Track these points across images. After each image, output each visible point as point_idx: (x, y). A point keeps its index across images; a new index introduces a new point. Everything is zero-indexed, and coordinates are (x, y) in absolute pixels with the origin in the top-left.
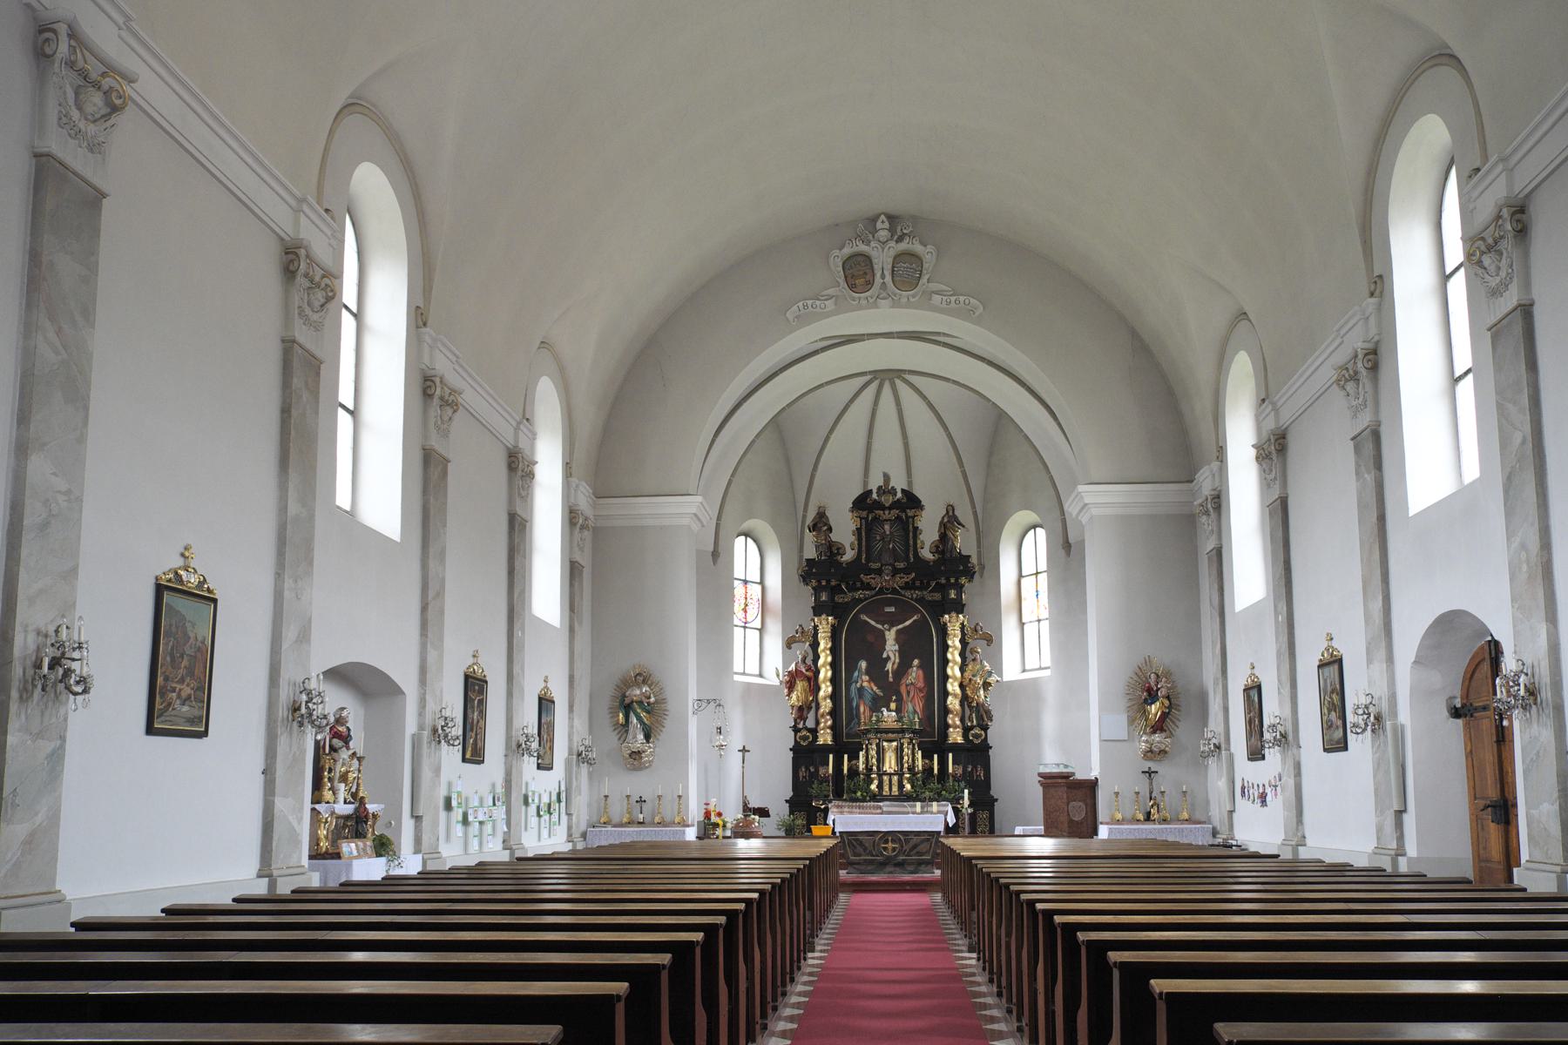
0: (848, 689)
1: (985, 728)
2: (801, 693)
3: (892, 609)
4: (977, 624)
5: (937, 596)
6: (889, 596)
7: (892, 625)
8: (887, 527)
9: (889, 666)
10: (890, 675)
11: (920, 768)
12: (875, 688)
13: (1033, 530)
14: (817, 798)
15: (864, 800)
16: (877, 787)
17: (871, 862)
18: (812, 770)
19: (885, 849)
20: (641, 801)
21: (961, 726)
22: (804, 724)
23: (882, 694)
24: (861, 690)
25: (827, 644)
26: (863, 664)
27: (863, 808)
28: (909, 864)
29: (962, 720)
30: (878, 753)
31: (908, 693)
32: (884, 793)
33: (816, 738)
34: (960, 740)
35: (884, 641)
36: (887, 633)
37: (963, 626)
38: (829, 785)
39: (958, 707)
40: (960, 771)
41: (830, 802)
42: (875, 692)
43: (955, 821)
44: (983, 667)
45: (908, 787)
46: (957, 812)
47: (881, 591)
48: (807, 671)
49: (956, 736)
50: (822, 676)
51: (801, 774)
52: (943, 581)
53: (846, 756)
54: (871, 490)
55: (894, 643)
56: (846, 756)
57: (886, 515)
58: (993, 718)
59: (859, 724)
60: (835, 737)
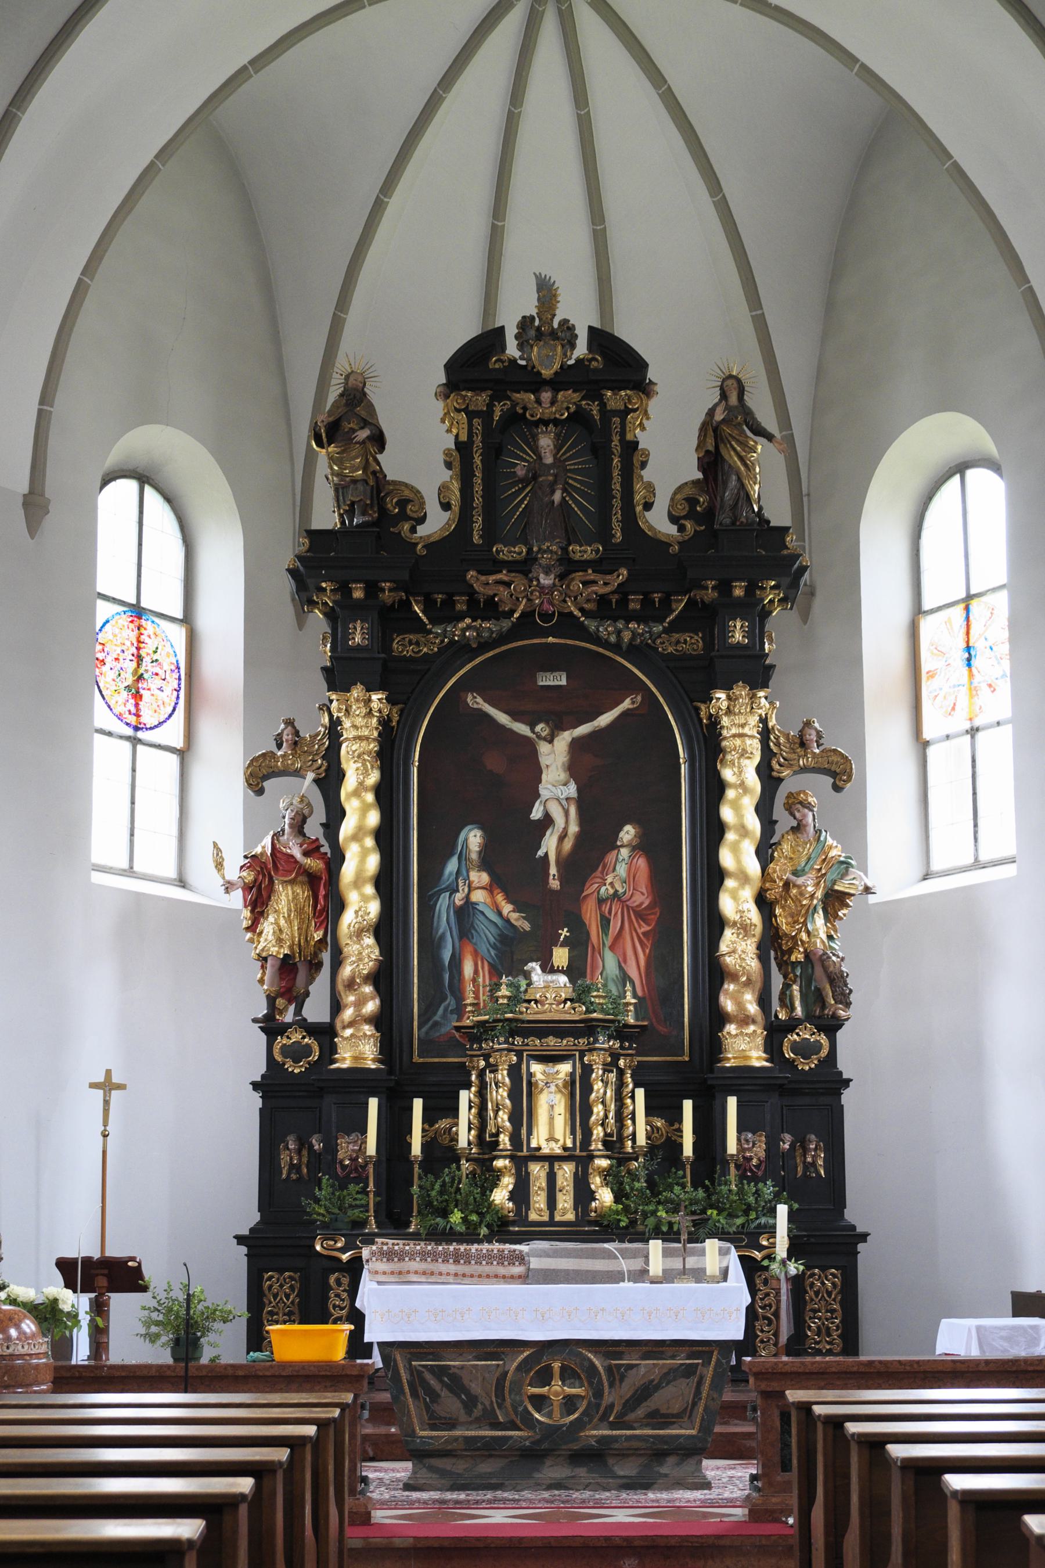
1: (831, 1026)
2: (289, 920)
4: (808, 724)
5: (692, 642)
6: (550, 639)
7: (558, 726)
8: (546, 442)
9: (549, 845)
10: (553, 870)
11: (642, 1140)
12: (507, 908)
13: (957, 478)
14: (330, 1230)
15: (470, 1236)
16: (513, 1196)
17: (488, 1448)
18: (317, 1146)
19: (540, 1402)
21: (760, 1018)
22: (298, 1011)
23: (526, 926)
24: (466, 913)
25: (366, 774)
26: (473, 839)
27: (467, 1258)
28: (623, 1455)
29: (763, 1001)
30: (514, 1094)
31: (605, 922)
32: (533, 1216)
33: (330, 1050)
34: (757, 1058)
36: (543, 748)
37: (765, 733)
38: (364, 1192)
39: (753, 964)
40: (759, 1151)
41: (369, 1240)
42: (507, 921)
43: (749, 1300)
44: (824, 850)
45: (605, 1197)
47: (527, 624)
48: (306, 854)
50: (348, 871)
51: (284, 1158)
52: (710, 594)
53: (418, 1104)
54: (502, 329)
55: (563, 776)
56: (418, 1104)
58: (852, 998)
59: (460, 1011)
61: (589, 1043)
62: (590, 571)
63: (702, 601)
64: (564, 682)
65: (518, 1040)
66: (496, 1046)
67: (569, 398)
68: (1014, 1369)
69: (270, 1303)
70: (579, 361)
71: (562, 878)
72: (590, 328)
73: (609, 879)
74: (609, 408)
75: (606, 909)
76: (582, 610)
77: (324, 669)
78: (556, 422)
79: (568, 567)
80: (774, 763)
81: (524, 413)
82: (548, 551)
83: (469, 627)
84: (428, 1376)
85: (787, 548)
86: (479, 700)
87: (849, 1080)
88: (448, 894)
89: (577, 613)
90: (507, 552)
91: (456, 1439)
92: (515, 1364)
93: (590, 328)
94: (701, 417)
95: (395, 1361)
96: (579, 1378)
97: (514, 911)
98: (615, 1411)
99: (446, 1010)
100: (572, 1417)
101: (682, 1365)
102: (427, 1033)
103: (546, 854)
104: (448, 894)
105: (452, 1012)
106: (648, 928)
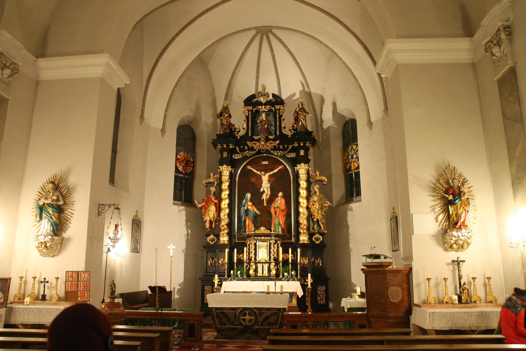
0: (239, 210)
3: (266, 163)
5: (293, 155)
6: (265, 155)
7: (266, 172)
9: (264, 197)
10: (265, 202)
12: (255, 210)
19: (244, 320)
20: (45, 281)
23: (259, 213)
24: (247, 211)
26: (249, 195)
30: (255, 249)
31: (276, 213)
32: (259, 275)
35: (261, 182)
36: (263, 177)
42: (256, 212)
46: (304, 286)
47: (259, 152)
49: (304, 238)
51: (209, 263)
52: (296, 145)
55: (267, 182)
56: (235, 250)
57: (263, 108)
59: (245, 231)
60: (230, 240)
64: (267, 163)
65: (256, 238)
70: (270, 100)
71: (267, 203)
73: (276, 203)
75: (276, 210)
76: (270, 149)
77: (219, 162)
80: (311, 179)
81: (259, 110)
83: (247, 153)
84: (220, 314)
85: (313, 135)
86: (250, 167)
87: (326, 246)
88: (243, 207)
90: (256, 138)
92: (239, 312)
95: (213, 310)
99: (243, 231)
100: (251, 324)
102: (239, 236)
103: (264, 198)
104: (243, 207)
106: (285, 214)
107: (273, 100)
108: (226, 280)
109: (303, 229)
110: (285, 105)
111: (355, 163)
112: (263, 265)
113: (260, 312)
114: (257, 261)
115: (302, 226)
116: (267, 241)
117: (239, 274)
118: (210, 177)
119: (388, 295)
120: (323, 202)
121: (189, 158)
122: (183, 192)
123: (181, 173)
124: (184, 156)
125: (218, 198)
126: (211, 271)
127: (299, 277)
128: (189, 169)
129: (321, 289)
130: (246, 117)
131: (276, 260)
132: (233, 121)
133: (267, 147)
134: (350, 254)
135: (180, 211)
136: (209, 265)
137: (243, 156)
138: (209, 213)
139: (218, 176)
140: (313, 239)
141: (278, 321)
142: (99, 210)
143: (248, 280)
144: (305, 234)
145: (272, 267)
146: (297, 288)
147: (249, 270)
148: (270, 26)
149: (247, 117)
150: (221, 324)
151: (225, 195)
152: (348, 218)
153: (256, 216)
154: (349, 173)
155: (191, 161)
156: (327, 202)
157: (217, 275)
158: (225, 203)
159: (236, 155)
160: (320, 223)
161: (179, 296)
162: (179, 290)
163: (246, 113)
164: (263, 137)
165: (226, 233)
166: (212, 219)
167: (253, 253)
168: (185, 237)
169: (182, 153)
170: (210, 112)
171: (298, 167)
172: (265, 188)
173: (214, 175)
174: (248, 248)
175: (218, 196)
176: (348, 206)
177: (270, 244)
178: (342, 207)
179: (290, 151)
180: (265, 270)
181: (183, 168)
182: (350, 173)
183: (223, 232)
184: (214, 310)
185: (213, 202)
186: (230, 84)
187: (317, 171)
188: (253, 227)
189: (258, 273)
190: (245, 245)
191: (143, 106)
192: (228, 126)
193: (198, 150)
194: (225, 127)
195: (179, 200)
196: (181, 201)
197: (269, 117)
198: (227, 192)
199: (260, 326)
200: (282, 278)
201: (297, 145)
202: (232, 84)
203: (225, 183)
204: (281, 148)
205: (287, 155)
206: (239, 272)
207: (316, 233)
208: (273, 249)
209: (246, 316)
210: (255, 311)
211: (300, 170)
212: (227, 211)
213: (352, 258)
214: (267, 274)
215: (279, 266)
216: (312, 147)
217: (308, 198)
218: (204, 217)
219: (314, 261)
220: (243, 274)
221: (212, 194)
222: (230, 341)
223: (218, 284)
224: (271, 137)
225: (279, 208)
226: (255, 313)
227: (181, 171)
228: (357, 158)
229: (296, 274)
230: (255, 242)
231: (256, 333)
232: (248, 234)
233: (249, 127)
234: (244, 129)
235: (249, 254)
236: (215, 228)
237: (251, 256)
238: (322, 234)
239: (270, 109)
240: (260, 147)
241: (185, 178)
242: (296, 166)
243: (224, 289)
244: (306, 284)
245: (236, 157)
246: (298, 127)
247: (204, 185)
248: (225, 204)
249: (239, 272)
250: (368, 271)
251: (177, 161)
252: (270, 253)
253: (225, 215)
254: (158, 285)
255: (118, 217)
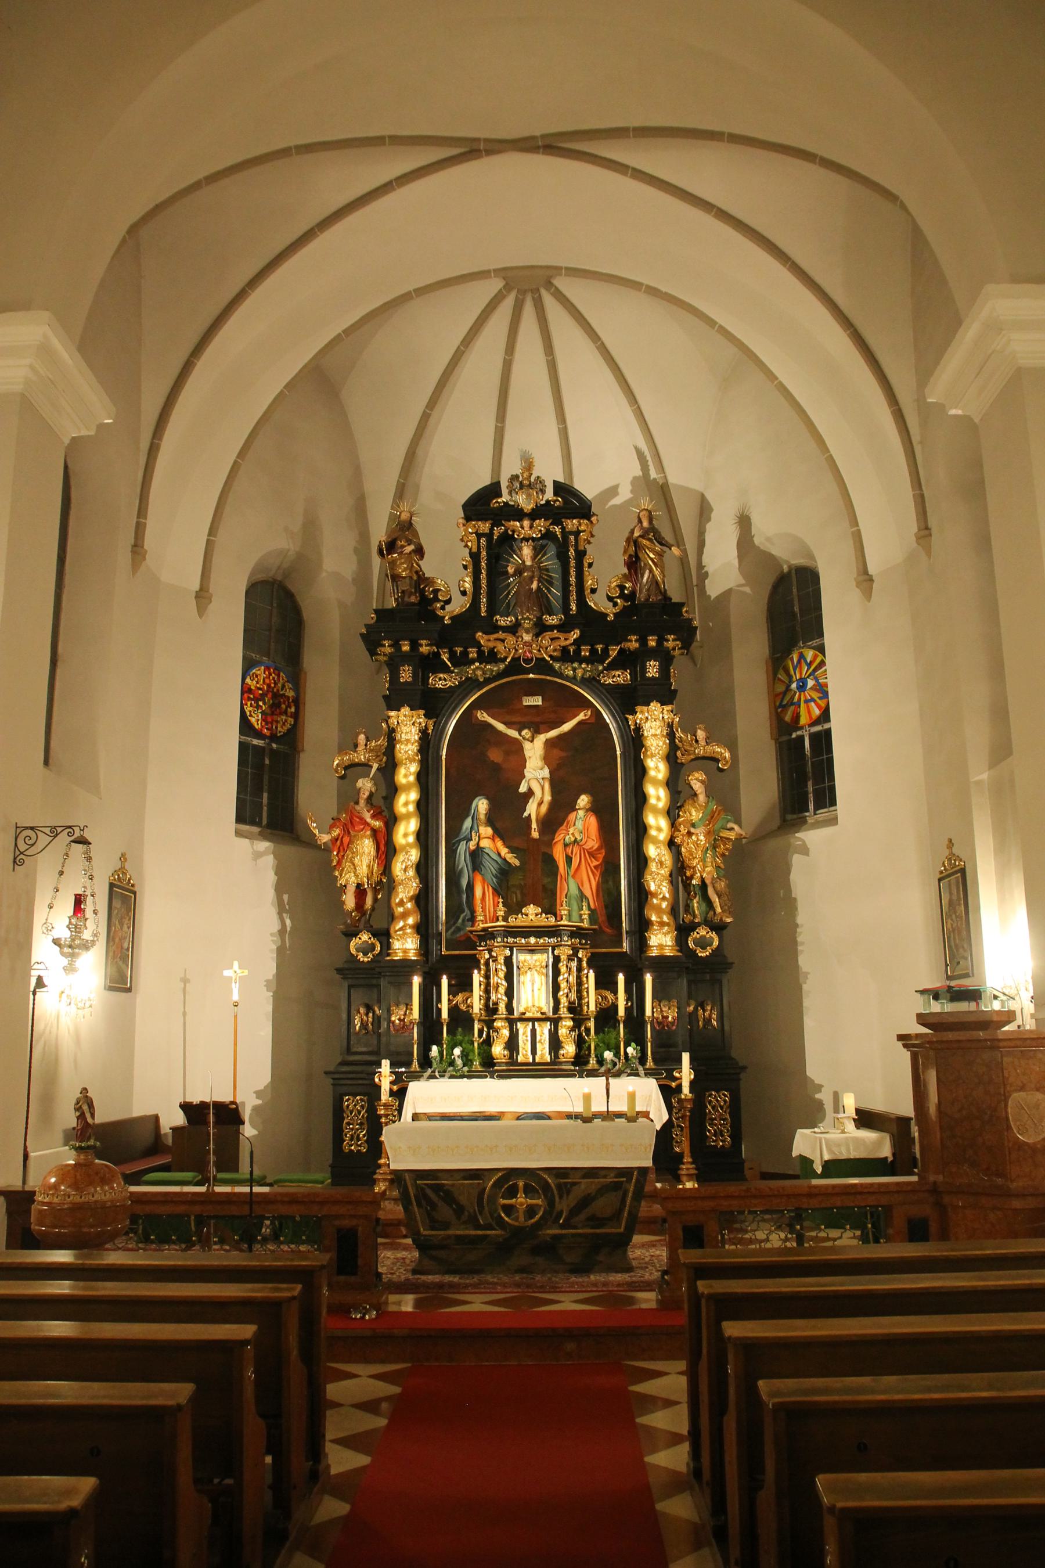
3: (537, 701)
5: (621, 677)
6: (531, 676)
7: (537, 731)
9: (532, 809)
10: (534, 825)
12: (504, 851)
19: (509, 1209)
23: (517, 863)
24: (476, 855)
26: (482, 805)
30: (509, 977)
31: (569, 860)
32: (520, 1059)
33: (387, 946)
36: (527, 745)
42: (505, 859)
46: (669, 1092)
47: (515, 667)
51: (357, 1021)
52: (633, 644)
55: (540, 763)
56: (445, 981)
57: (523, 528)
58: (810, 853)
59: (473, 919)
60: (425, 948)
61: (558, 942)
62: (555, 632)
63: (629, 648)
64: (540, 703)
65: (511, 940)
66: (496, 944)
67: (541, 524)
68: (853, 1191)
69: (348, 1117)
70: (548, 502)
71: (541, 832)
72: (555, 482)
73: (571, 831)
74: (567, 530)
75: (569, 850)
76: (551, 656)
78: (533, 539)
79: (541, 628)
80: (679, 754)
81: (513, 535)
82: (528, 618)
83: (477, 668)
84: (429, 1192)
86: (485, 715)
89: (547, 658)
90: (503, 621)
91: (449, 1237)
93: (555, 482)
94: (626, 534)
95: (405, 1180)
96: (538, 1192)
97: (508, 853)
98: (564, 1216)
99: (463, 920)
100: (533, 1221)
101: (611, 1182)
102: (453, 933)
103: (530, 815)
104: (465, 842)
105: (468, 920)
106: (598, 863)
107: (558, 503)
108: (416, 1076)
109: (659, 910)
110: (594, 519)
111: (813, 704)
112: (533, 1025)
113: (562, 1181)
114: (516, 1015)
115: (655, 901)
116: (547, 951)
117: (458, 1057)
118: (356, 746)
119: (1007, 1119)
120: (717, 827)
121: (283, 686)
122: (265, 795)
123: (258, 734)
124: (267, 681)
125: (383, 813)
126: (364, 1049)
127: (650, 1064)
128: (284, 724)
129: (717, 1101)
130: (471, 554)
131: (576, 1010)
132: (428, 567)
133: (539, 651)
134: (800, 989)
135: (257, 855)
136: (357, 1028)
137: (461, 678)
138: (356, 861)
139: (382, 742)
140: (691, 944)
141: (621, 1210)
142: (16, 845)
143: (486, 1077)
144: (666, 928)
145: (563, 1032)
146: (650, 1100)
147: (488, 1043)
148: (548, 267)
149: (475, 557)
150: (434, 1224)
151: (406, 804)
152: (792, 877)
153: (505, 872)
154: (791, 735)
155: (288, 698)
156: (730, 825)
157: (388, 1062)
158: (406, 828)
159: (442, 675)
160: (711, 892)
161: (257, 1130)
162: (256, 1109)
163: (469, 544)
164: (530, 620)
165: (412, 927)
166: (365, 880)
167: (502, 990)
168: (275, 939)
169: (260, 671)
170: (350, 540)
171: (639, 715)
172: (536, 782)
173: (368, 739)
174: (482, 972)
175: (384, 808)
176: (792, 840)
177: (557, 960)
178: (773, 844)
179: (613, 666)
180: (540, 1041)
181: (263, 720)
182: (794, 736)
183: (401, 924)
184: (407, 1177)
185: (367, 827)
186: (414, 453)
187: (700, 728)
188: (501, 905)
189: (518, 1053)
190: (474, 962)
191: (142, 511)
192: (413, 582)
193: (312, 661)
194: (405, 586)
195: (252, 823)
196: (258, 824)
197: (542, 557)
198: (414, 795)
199: (562, 1229)
200: (596, 1066)
201: (637, 645)
202: (420, 452)
203: (406, 764)
204: (583, 654)
205: (604, 677)
206: (457, 1051)
207: (699, 925)
208: (566, 976)
209: (516, 1197)
210: (545, 1179)
211: (648, 725)
212: (414, 855)
213: (806, 1003)
214: (549, 1057)
215: (583, 1028)
216: (681, 651)
217: (673, 813)
218: (337, 873)
219: (693, 1011)
220: (470, 1057)
221: (362, 802)
222: (468, 1281)
223: (391, 1090)
224: (552, 620)
225: (581, 843)
226: (546, 1187)
227: (257, 727)
228: (822, 690)
229: (639, 1055)
230: (508, 952)
231: (549, 1250)
232: (485, 930)
233: (480, 588)
234: (464, 593)
235: (487, 991)
236: (373, 909)
237: (493, 997)
238: (719, 928)
239: (548, 530)
240: (517, 650)
241: (272, 750)
242: (634, 713)
243: (415, 1108)
244: (674, 1084)
245: (440, 682)
246: (638, 589)
247: (336, 771)
248: (406, 831)
249: (457, 1051)
250: (937, 1042)
251: (246, 695)
252: (556, 988)
253: (406, 867)
254: (213, 1100)
255: (85, 870)
